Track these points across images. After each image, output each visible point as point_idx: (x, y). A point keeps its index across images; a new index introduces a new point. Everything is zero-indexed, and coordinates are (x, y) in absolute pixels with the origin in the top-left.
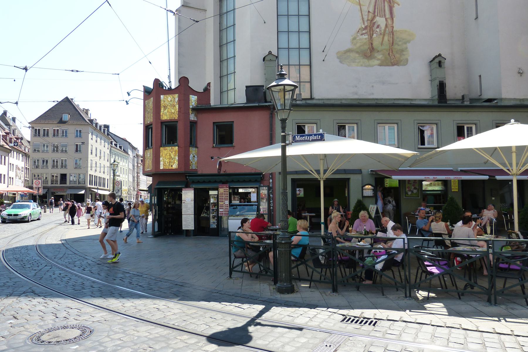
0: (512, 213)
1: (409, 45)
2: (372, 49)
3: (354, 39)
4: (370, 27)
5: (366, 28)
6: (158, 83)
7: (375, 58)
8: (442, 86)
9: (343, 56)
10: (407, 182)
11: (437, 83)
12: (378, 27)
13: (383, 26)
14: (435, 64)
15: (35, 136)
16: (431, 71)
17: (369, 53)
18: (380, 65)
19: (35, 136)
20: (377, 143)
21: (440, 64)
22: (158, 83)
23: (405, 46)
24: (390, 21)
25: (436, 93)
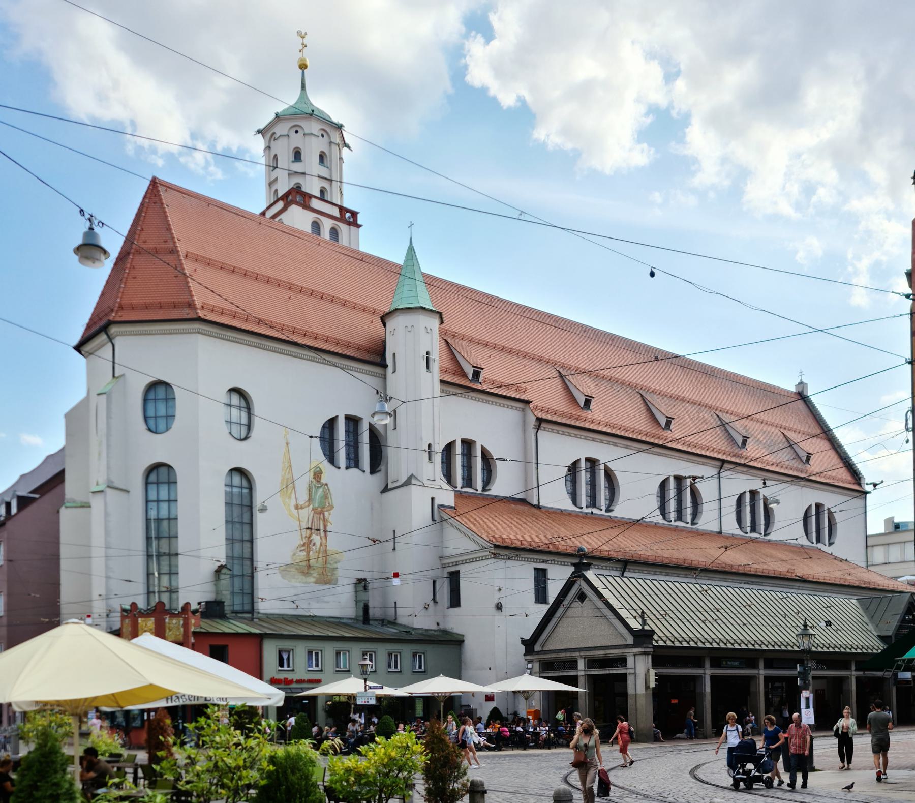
0: (766, 694)
1: (339, 565)
2: (309, 566)
3: (294, 555)
4: (307, 544)
5: (304, 545)
6: (134, 605)
7: (311, 574)
8: (366, 608)
9: (285, 569)
10: (179, 710)
11: (362, 605)
12: (314, 544)
13: (318, 544)
14: (360, 588)
15: (486, 696)
16: (356, 592)
17: (306, 569)
18: (316, 583)
19: (486, 696)
20: (460, 678)
21: (365, 588)
22: (134, 605)
23: (335, 566)
24: (324, 541)
25: (361, 613)
